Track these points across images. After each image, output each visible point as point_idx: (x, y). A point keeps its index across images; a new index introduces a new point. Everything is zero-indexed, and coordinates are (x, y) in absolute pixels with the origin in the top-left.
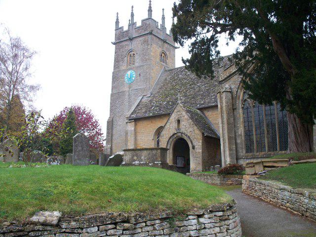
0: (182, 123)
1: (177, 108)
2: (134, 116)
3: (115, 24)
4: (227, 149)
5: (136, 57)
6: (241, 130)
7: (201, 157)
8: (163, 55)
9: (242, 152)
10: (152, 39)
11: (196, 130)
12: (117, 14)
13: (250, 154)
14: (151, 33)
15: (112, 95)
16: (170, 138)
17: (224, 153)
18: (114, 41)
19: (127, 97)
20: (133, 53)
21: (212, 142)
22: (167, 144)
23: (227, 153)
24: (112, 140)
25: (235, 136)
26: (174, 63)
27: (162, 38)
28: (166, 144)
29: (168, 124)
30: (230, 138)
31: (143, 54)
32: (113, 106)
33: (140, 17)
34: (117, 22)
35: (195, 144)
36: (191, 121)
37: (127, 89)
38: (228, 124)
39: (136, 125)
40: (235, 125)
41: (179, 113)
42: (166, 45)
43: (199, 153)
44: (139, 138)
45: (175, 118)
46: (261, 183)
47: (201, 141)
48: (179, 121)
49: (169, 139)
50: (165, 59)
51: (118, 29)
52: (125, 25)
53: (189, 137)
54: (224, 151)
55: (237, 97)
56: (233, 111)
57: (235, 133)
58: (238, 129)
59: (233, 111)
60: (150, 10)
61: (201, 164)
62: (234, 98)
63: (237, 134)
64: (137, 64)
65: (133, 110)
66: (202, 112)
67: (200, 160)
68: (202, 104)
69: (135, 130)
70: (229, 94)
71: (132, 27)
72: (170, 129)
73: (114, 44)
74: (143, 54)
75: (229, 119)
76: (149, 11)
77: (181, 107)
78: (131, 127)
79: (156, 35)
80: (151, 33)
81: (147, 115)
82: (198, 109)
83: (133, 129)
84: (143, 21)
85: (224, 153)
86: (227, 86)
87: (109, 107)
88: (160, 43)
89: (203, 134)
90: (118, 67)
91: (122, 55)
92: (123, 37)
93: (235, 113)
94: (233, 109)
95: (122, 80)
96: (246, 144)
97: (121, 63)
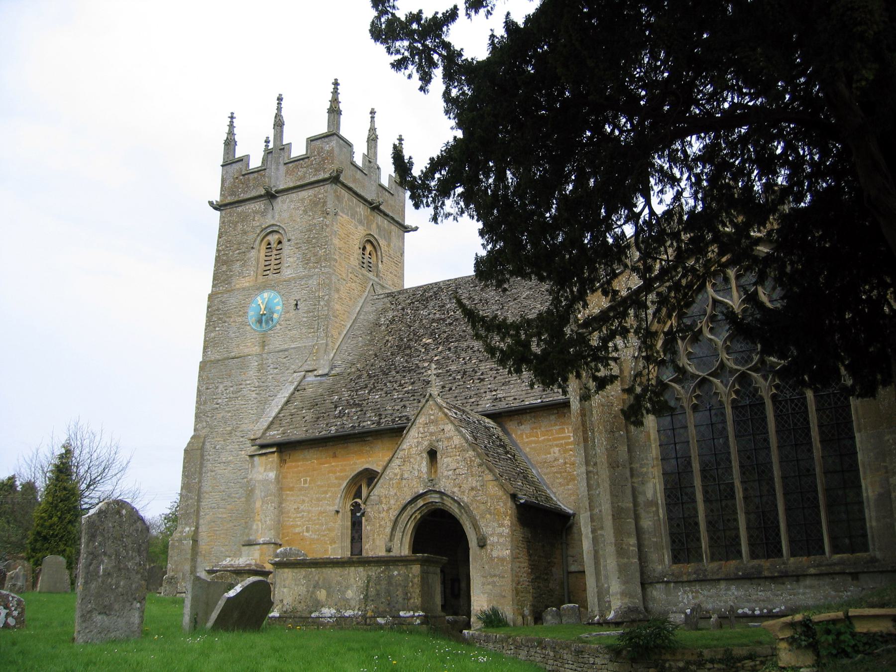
0: (445, 462)
2: (276, 435)
5: (287, 249)
6: (653, 487)
7: (508, 576)
8: (369, 248)
13: (690, 567)
16: (404, 508)
18: (216, 197)
19: (252, 373)
21: (544, 526)
22: (394, 529)
24: (198, 512)
25: (635, 504)
26: (401, 277)
28: (388, 530)
29: (396, 462)
30: (618, 514)
31: (308, 241)
32: (205, 403)
34: (230, 143)
35: (486, 530)
36: (471, 453)
37: (257, 349)
38: (613, 465)
40: (631, 470)
41: (432, 428)
42: (379, 219)
43: (502, 560)
44: (290, 506)
47: (507, 522)
48: (432, 454)
50: (374, 258)
58: (643, 483)
60: (334, 111)
63: (641, 499)
64: (287, 273)
66: (500, 425)
69: (278, 480)
73: (217, 207)
74: (308, 241)
78: (265, 471)
80: (335, 179)
82: (488, 416)
83: (272, 475)
84: (311, 141)
89: (514, 497)
95: (240, 319)
97: (237, 266)
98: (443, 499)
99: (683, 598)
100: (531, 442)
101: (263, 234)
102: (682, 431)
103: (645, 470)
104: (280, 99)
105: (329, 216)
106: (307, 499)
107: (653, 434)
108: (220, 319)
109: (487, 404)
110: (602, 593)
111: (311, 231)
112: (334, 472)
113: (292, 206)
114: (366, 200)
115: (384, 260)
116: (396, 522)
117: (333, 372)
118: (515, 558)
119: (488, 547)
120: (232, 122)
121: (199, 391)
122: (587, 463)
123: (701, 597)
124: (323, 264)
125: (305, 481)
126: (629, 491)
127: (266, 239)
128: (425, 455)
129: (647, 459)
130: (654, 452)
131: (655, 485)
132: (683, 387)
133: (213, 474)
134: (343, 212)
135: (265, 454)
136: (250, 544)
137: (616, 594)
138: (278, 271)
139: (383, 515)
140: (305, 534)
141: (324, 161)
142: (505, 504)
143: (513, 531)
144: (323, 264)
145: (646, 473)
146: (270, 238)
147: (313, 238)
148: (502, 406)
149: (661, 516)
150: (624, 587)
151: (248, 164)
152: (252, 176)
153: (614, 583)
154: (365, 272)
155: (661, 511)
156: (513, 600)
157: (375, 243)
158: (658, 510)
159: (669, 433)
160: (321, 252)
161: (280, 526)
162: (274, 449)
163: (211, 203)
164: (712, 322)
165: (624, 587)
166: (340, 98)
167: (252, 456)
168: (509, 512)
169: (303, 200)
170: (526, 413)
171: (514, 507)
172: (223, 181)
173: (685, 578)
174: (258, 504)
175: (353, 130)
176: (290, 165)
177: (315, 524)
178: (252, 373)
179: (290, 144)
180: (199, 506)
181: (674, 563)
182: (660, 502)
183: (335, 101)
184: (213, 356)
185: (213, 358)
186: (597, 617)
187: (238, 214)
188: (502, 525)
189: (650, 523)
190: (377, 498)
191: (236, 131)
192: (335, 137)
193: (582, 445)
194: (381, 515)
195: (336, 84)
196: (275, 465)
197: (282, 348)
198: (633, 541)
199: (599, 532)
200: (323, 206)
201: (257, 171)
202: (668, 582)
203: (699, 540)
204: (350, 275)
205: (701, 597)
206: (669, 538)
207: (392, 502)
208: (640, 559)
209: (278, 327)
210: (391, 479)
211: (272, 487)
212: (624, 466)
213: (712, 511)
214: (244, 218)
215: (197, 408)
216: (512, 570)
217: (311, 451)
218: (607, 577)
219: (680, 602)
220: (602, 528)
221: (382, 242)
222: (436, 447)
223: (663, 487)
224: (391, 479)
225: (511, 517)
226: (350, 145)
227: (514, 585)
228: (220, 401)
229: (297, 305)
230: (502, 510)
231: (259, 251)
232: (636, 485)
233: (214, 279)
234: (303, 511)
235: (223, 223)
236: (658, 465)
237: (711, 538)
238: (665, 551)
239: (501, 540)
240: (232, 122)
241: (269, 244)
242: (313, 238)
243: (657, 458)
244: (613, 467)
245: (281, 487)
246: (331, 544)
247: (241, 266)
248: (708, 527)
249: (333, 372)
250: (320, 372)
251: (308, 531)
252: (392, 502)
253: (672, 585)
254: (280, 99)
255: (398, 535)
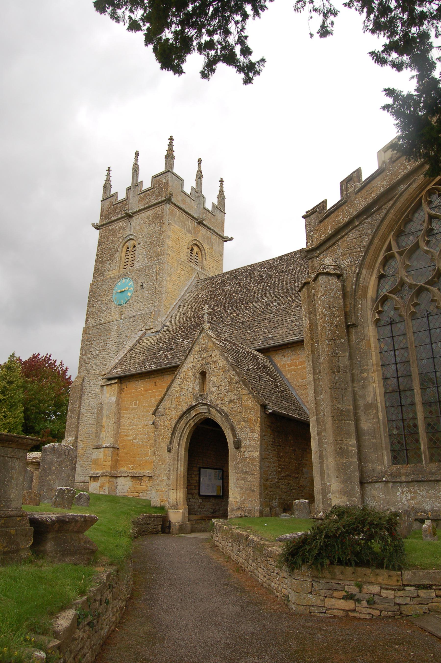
0: (211, 379)
1: (200, 341)
2: (119, 372)
3: (102, 189)
4: (329, 450)
5: (138, 249)
6: (374, 390)
7: (257, 473)
8: (196, 249)
9: (381, 462)
10: (171, 213)
11: (245, 398)
12: (109, 170)
13: (409, 468)
14: (168, 200)
15: (85, 331)
16: (181, 418)
17: (321, 463)
18: (97, 221)
19: (114, 333)
20: (132, 242)
21: (287, 432)
22: (173, 434)
23: (331, 462)
24: (78, 426)
25: (356, 408)
26: (222, 269)
27: (195, 215)
28: (169, 435)
30: (338, 415)
31: (151, 243)
32: (85, 355)
33: (152, 166)
34: (107, 186)
35: (241, 435)
36: (232, 372)
37: (117, 317)
38: (335, 370)
39: (121, 391)
40: (353, 375)
41: (204, 354)
42: (203, 230)
43: (252, 459)
44: (125, 421)
45: (194, 366)
46: (121, 243)
47: (257, 429)
48: (203, 374)
49: (178, 422)
50: (199, 258)
51: (108, 195)
52: (120, 188)
53: (226, 416)
54: (321, 457)
55: (359, 290)
56: (348, 332)
57: (355, 400)
58: (364, 387)
59: (348, 332)
60: (170, 156)
61: (257, 489)
62: (349, 297)
63: (361, 403)
64: (138, 265)
65: (120, 358)
66: (269, 358)
67: (255, 480)
68: (270, 339)
69: (118, 403)
70: (335, 283)
71: (134, 191)
72: (183, 389)
73: (97, 227)
74: (151, 243)
75: (335, 354)
76: (167, 157)
77: (210, 337)
78: (110, 396)
79: (183, 207)
81: (144, 369)
82: (258, 351)
83: (114, 399)
84: (154, 177)
85: (321, 463)
86: (328, 261)
87: (78, 356)
88: (190, 224)
89: (264, 407)
90: (102, 274)
91: (110, 249)
92: (116, 213)
93: (353, 337)
94: (348, 327)
95: (107, 298)
96: (429, 425)
97: (107, 264)
98: (209, 410)
99: (402, 499)
100: (291, 370)
101: (124, 242)
102: (401, 338)
103: (365, 375)
104: (137, 154)
105: (164, 226)
106: (136, 416)
107: (373, 342)
108: (96, 299)
109: (260, 344)
110: (325, 491)
111: (152, 236)
112: (145, 394)
113: (142, 222)
114: (193, 217)
115: (207, 258)
116: (175, 429)
117: (163, 329)
118: (263, 459)
119: (242, 449)
120: (109, 174)
121: (82, 347)
122: (314, 373)
123: (419, 497)
124: (160, 258)
125: (136, 403)
126: (350, 394)
127: (126, 245)
128: (198, 376)
129: (367, 365)
130: (374, 358)
131: (375, 389)
132: (402, 298)
133: (88, 401)
134: (175, 223)
135: (110, 384)
136: (98, 447)
137: (336, 492)
138: (132, 265)
139: (167, 423)
140: (134, 441)
141: (162, 190)
142: (256, 413)
143: (262, 437)
144: (160, 258)
145: (367, 378)
146: (128, 244)
147: (154, 241)
148: (272, 343)
149: (381, 418)
150: (342, 486)
151: (117, 198)
152: (118, 205)
153: (333, 481)
154: (192, 265)
155: (380, 414)
156: (261, 494)
157: (200, 246)
158: (377, 413)
159: (389, 340)
160: (159, 250)
161: (117, 435)
162: (116, 381)
163: (93, 225)
164: (428, 236)
165: (342, 486)
166: (174, 148)
167: (102, 386)
168: (259, 419)
169: (148, 217)
170: (288, 348)
171: (264, 416)
172: (102, 210)
173: (404, 479)
174: (104, 420)
175: (185, 169)
176: (142, 195)
177: (141, 434)
178: (114, 333)
179: (142, 182)
180: (78, 423)
181: (394, 464)
182: (379, 405)
183: (170, 151)
184: (92, 323)
185: (91, 325)
186: (321, 513)
187: (110, 230)
188: (253, 431)
189: (370, 425)
190: (163, 410)
191: (111, 179)
192: (170, 173)
193: (311, 356)
194: (166, 424)
195: (171, 139)
196: (116, 392)
197: (133, 314)
198: (353, 441)
199: (323, 434)
200: (161, 219)
201: (122, 202)
202: (387, 482)
203: (417, 441)
204: (180, 266)
205: (419, 497)
206: (388, 440)
207: (173, 413)
208: (360, 459)
209: (131, 301)
210: (173, 395)
211: (113, 407)
212: (345, 372)
213: (431, 412)
214: (113, 232)
215: (81, 358)
216: (261, 468)
217: (140, 382)
218: (329, 476)
219: (398, 502)
220: (325, 430)
221: (205, 246)
222: (205, 369)
223: (383, 391)
224: (173, 395)
225: (261, 424)
226: (182, 180)
227: (263, 481)
228: (94, 352)
229: (142, 286)
230: (254, 418)
231: (121, 252)
232: (356, 389)
233: (94, 274)
234: (133, 425)
235: (101, 237)
236: (377, 371)
237: (430, 440)
238: (384, 452)
239: (253, 443)
240: (109, 174)
241: (128, 248)
242: (154, 241)
243: (377, 365)
244: (334, 372)
245: (119, 408)
246: (150, 448)
247: (110, 264)
248: (427, 428)
249: (163, 329)
250: (155, 330)
251: (136, 439)
252: (173, 413)
253: (391, 485)
254: (137, 154)
255: (176, 439)
